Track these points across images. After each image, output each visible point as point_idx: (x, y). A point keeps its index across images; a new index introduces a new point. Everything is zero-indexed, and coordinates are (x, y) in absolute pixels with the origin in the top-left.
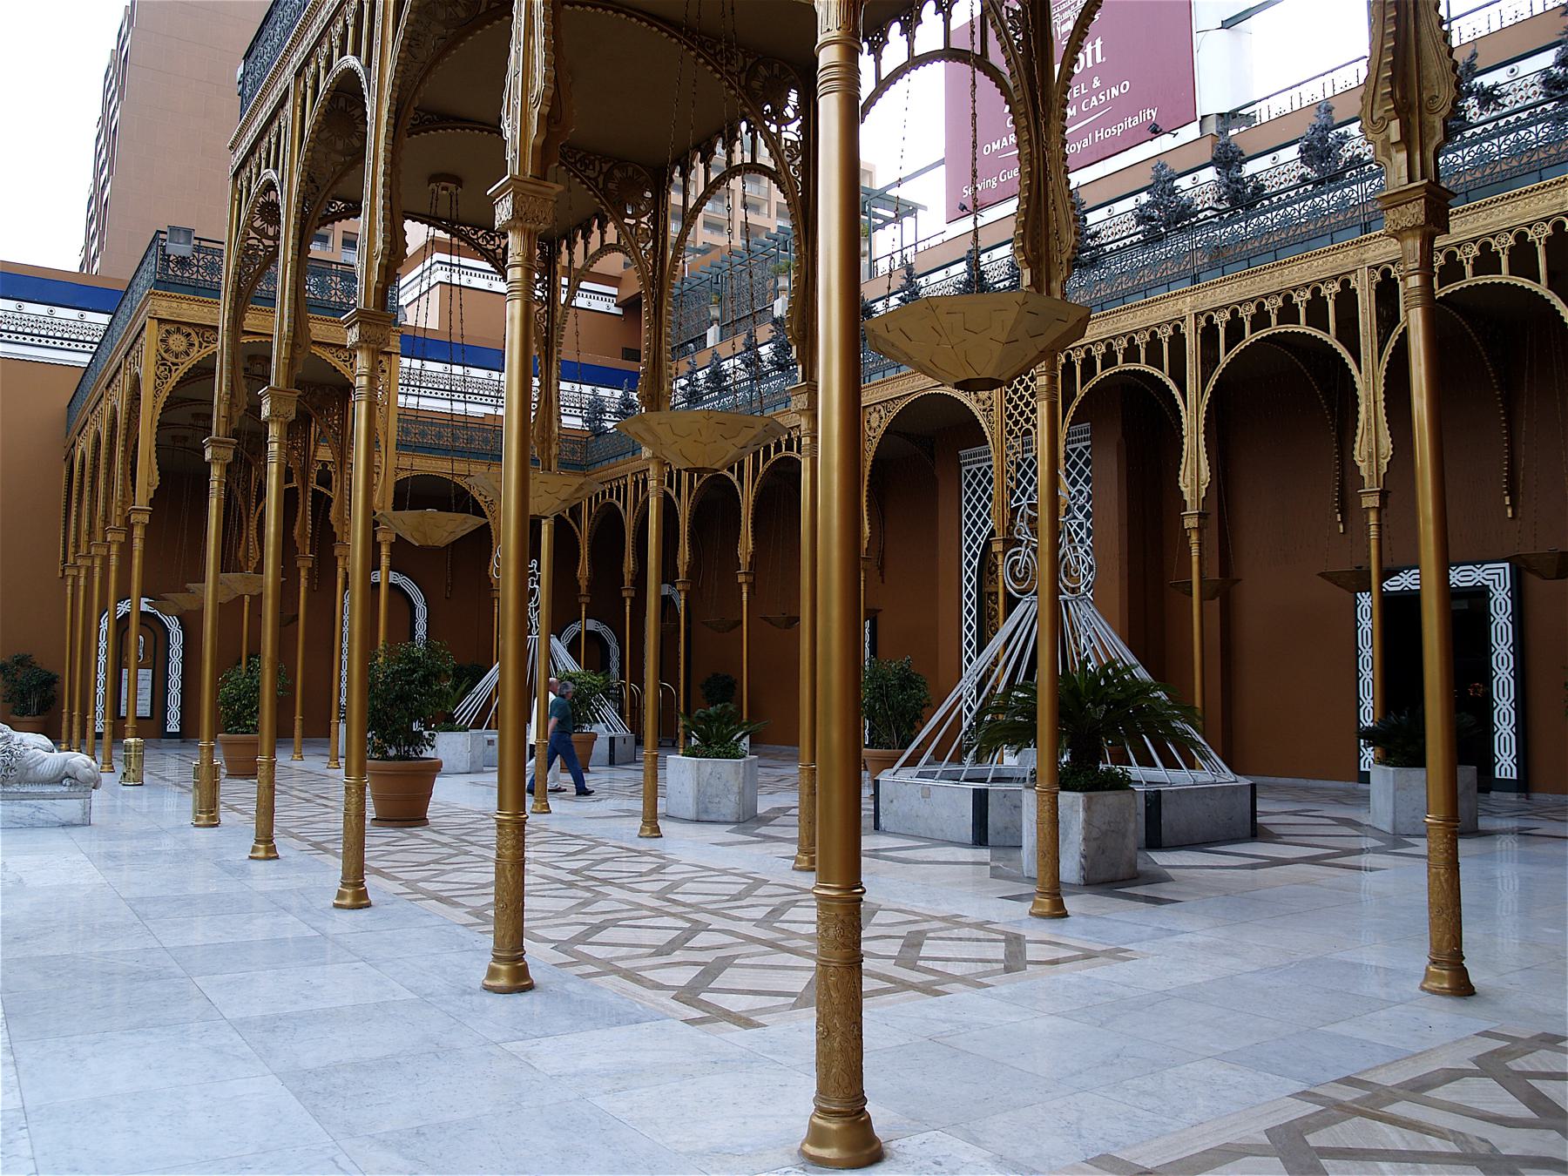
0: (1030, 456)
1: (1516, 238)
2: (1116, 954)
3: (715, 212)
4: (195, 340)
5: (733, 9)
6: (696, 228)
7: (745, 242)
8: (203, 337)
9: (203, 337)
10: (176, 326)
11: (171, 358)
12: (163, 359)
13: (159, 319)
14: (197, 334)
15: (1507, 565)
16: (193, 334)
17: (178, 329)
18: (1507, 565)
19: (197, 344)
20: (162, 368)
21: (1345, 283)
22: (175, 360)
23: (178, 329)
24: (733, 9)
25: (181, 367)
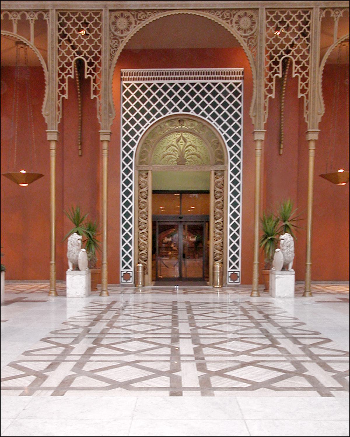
0: (115, 49)
1: (326, 13)
2: (320, 20)
3: (302, 219)
4: (132, 19)
5: (88, 419)
6: (328, 347)
7: (316, 388)
8: (137, 17)
9: (137, 17)
10: (244, 12)
11: (118, 34)
12: (114, 35)
13: (110, 10)
14: (133, 15)
15: (228, 283)
16: (131, 16)
17: (246, 14)
18: (228, 283)
19: (133, 22)
20: (114, 41)
21: (23, 16)
22: (234, 22)
23: (122, 15)
24: (88, 419)
25: (125, 39)
